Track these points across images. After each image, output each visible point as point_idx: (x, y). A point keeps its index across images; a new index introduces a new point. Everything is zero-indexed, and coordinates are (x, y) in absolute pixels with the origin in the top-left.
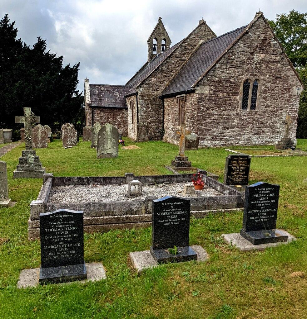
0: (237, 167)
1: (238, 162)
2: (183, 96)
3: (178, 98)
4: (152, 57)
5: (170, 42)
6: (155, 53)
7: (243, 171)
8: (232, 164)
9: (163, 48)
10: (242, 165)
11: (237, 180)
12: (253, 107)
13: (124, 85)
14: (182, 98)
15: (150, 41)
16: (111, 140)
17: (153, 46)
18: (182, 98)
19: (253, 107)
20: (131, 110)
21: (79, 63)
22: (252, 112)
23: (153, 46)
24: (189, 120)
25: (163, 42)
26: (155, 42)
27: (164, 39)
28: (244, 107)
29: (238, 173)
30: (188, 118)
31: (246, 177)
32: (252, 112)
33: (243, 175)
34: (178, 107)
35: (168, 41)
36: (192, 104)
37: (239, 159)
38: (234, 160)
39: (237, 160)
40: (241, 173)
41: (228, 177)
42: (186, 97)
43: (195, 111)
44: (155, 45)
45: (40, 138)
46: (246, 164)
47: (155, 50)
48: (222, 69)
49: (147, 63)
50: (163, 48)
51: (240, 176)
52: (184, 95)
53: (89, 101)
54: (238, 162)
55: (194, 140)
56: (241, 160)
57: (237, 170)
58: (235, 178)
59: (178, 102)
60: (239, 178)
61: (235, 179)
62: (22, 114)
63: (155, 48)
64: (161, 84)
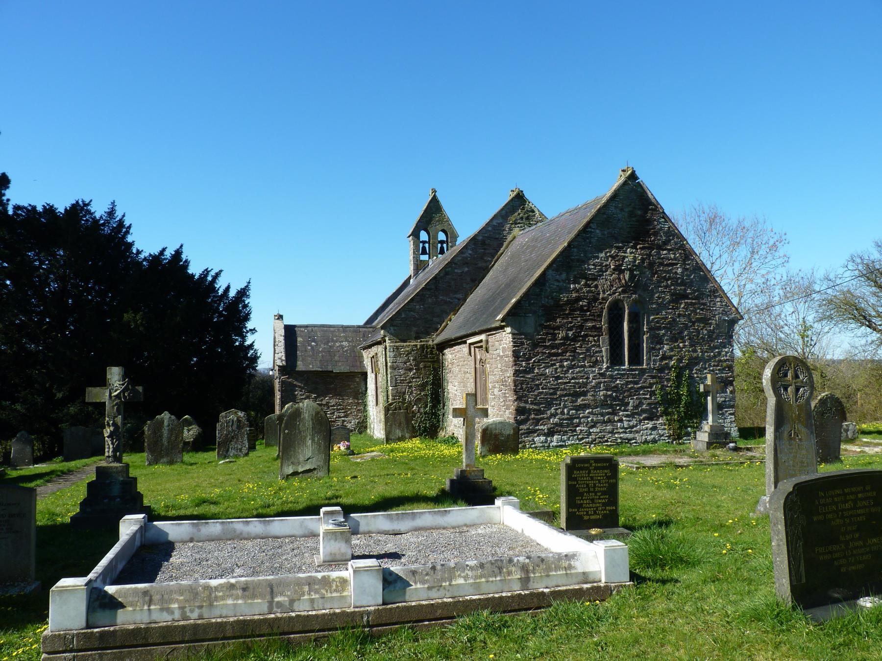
0: (588, 485)
1: (589, 473)
2: (481, 341)
3: (472, 347)
4: (419, 266)
5: (455, 237)
6: (424, 258)
7: (604, 493)
8: (575, 479)
9: (442, 248)
10: (599, 481)
11: (592, 517)
12: (636, 358)
13: (361, 322)
14: (479, 345)
15: (415, 234)
16: (313, 440)
17: (421, 245)
18: (479, 345)
19: (636, 358)
20: (373, 376)
21: (113, 203)
22: (634, 370)
23: (421, 245)
24: (496, 391)
25: (442, 236)
26: (424, 236)
27: (444, 231)
28: (616, 358)
29: (593, 500)
30: (494, 387)
31: (612, 508)
32: (634, 370)
33: (604, 504)
34: (473, 363)
35: (451, 235)
36: (501, 357)
37: (591, 465)
38: (580, 469)
39: (587, 468)
40: (600, 499)
41: (571, 510)
42: (487, 342)
43: (507, 371)
44: (424, 242)
45: (166, 443)
46: (608, 478)
47: (424, 252)
48: (558, 281)
49: (410, 277)
50: (442, 248)
51: (597, 508)
52: (483, 337)
53: (282, 361)
54: (589, 473)
55: (509, 435)
56: (596, 468)
57: (589, 492)
58: (587, 512)
59: (473, 354)
60: (595, 512)
61: (587, 514)
62: (102, 382)
63: (424, 248)
64: (435, 319)
